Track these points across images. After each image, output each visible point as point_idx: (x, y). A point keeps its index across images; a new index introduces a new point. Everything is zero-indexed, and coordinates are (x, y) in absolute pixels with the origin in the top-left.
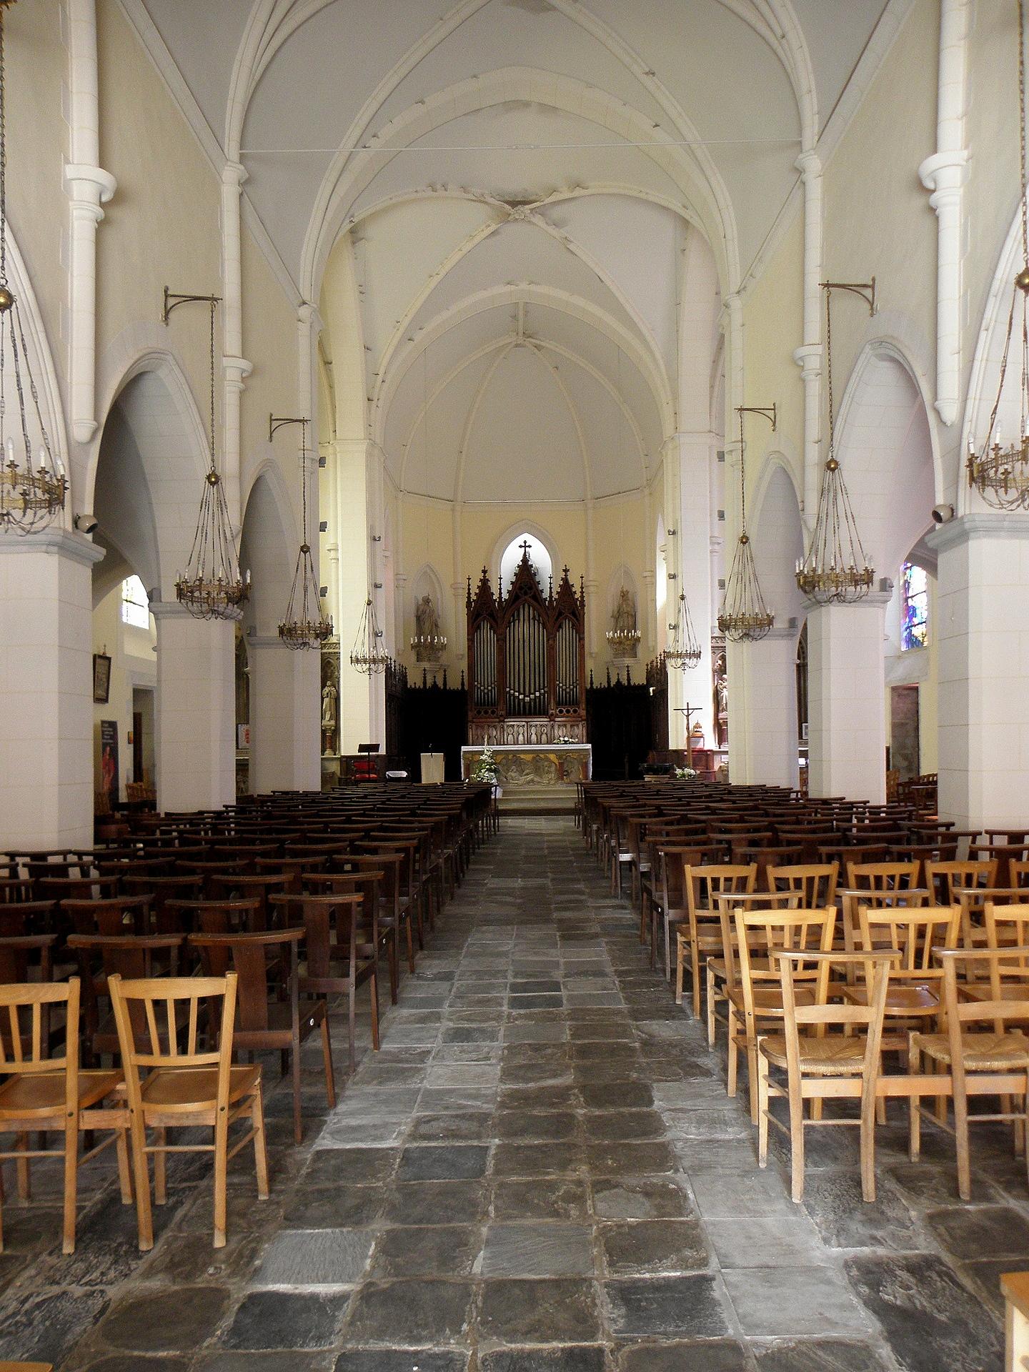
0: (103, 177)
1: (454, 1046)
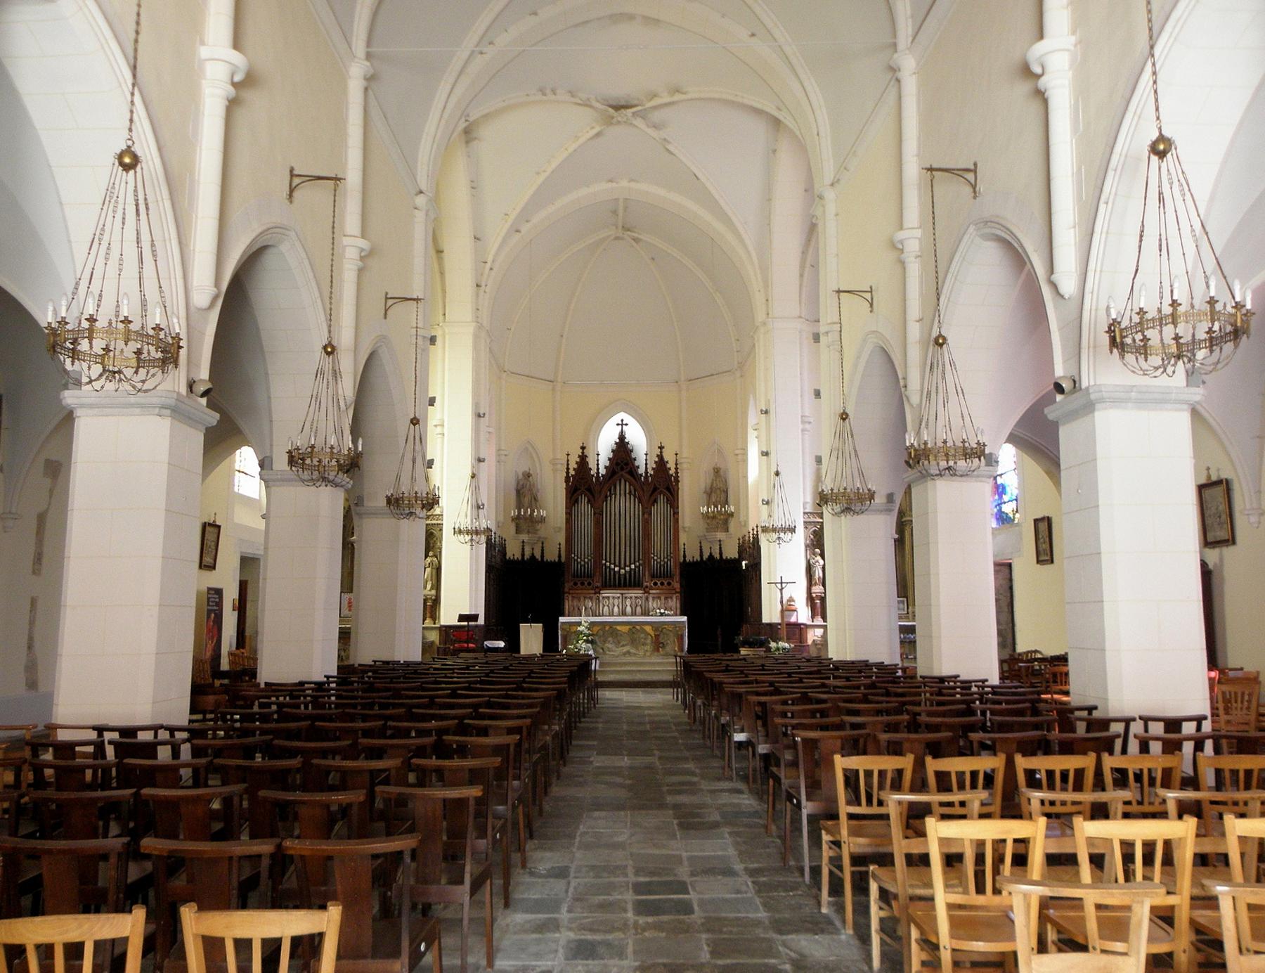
0: (237, 58)
1: (577, 966)
